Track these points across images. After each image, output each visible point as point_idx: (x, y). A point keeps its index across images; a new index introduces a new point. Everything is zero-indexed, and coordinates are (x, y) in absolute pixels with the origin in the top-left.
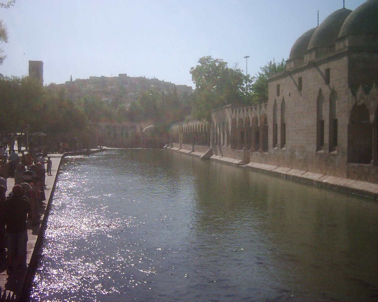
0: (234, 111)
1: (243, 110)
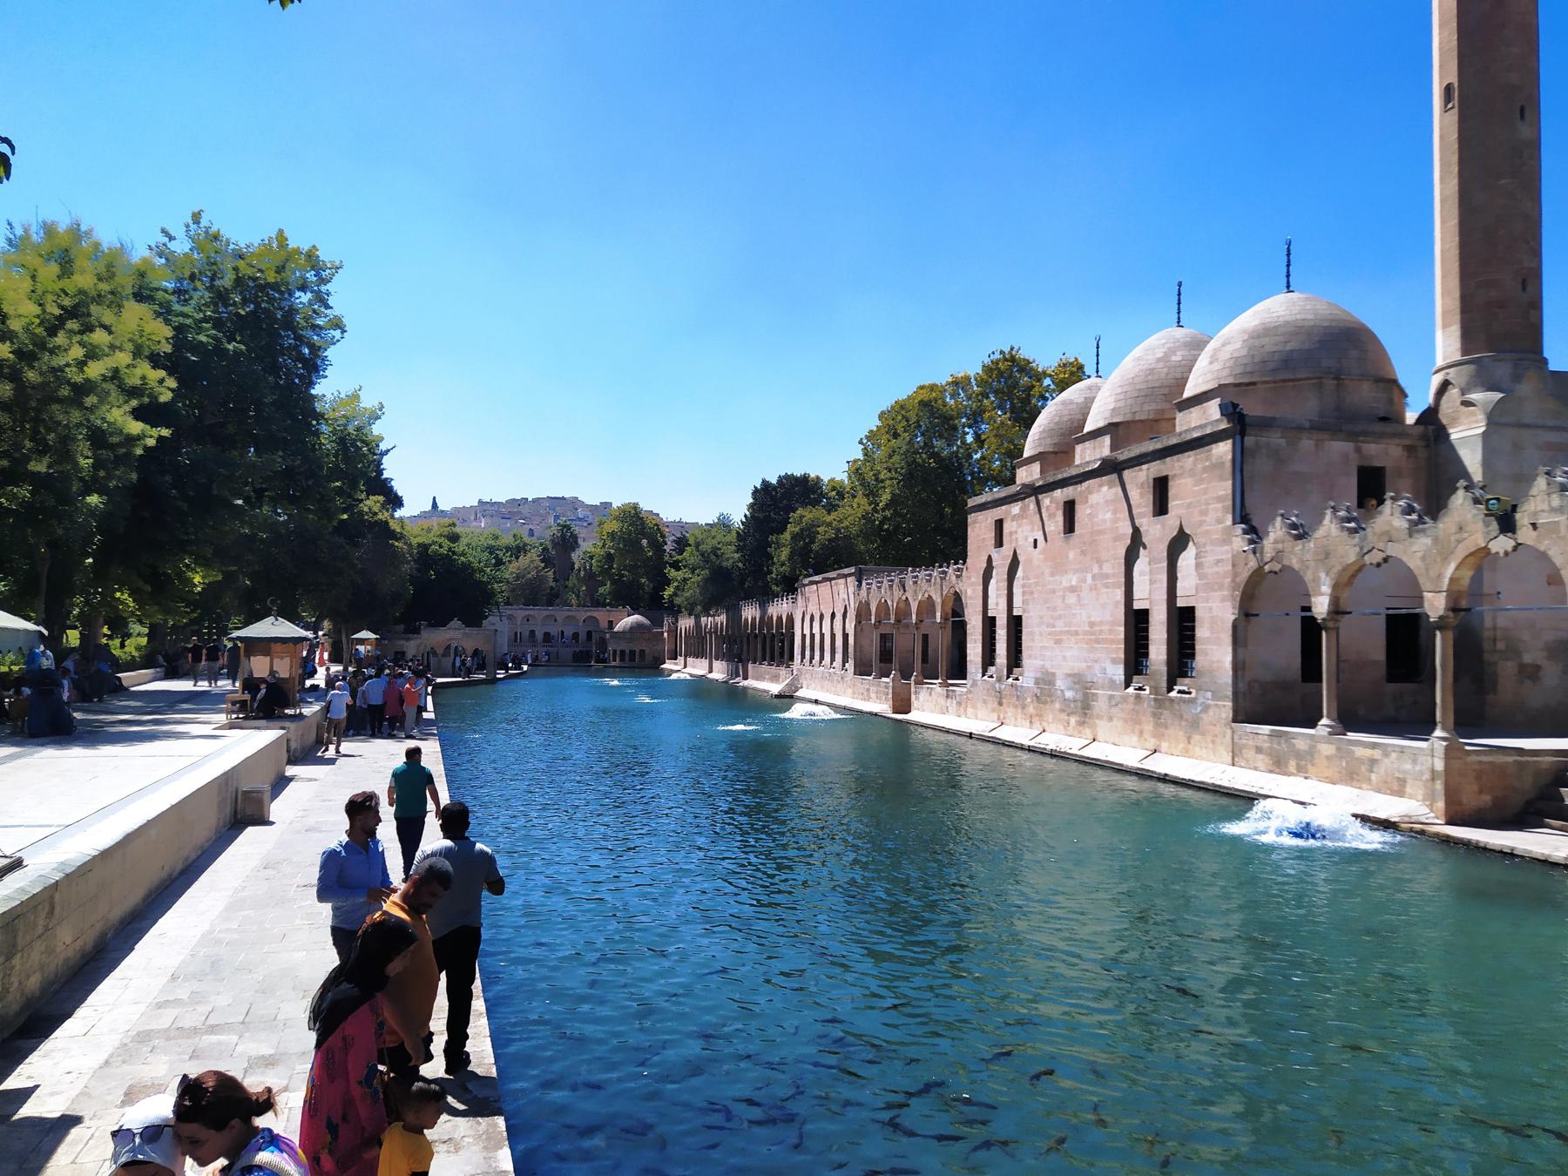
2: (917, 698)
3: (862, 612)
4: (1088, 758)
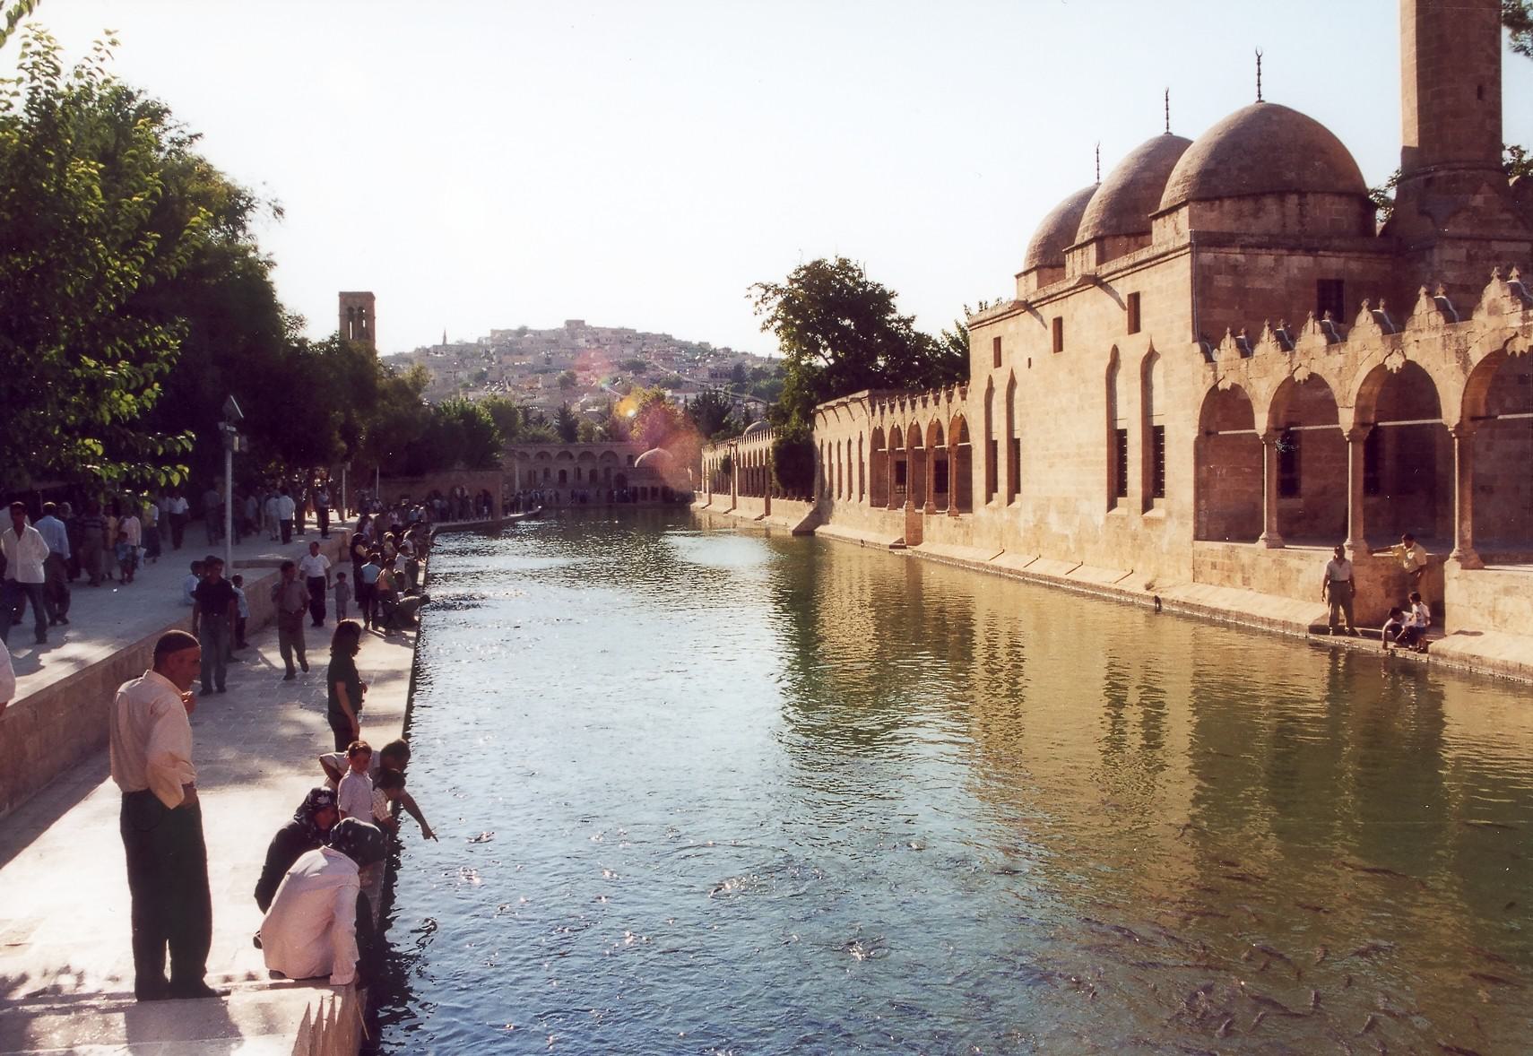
0: (878, 407)
1: (892, 407)
2: (929, 529)
3: (878, 436)
4: (1091, 586)
